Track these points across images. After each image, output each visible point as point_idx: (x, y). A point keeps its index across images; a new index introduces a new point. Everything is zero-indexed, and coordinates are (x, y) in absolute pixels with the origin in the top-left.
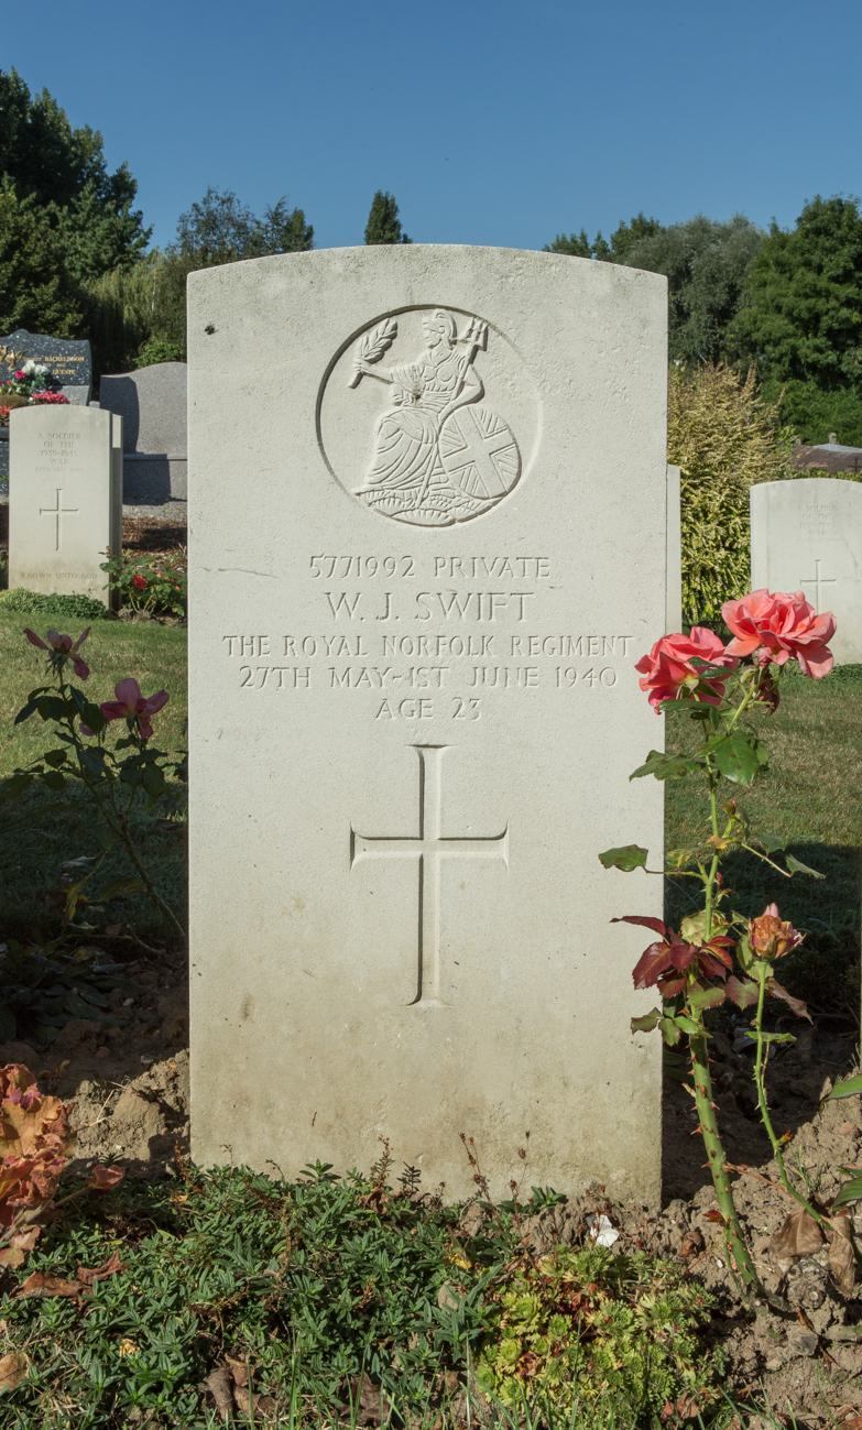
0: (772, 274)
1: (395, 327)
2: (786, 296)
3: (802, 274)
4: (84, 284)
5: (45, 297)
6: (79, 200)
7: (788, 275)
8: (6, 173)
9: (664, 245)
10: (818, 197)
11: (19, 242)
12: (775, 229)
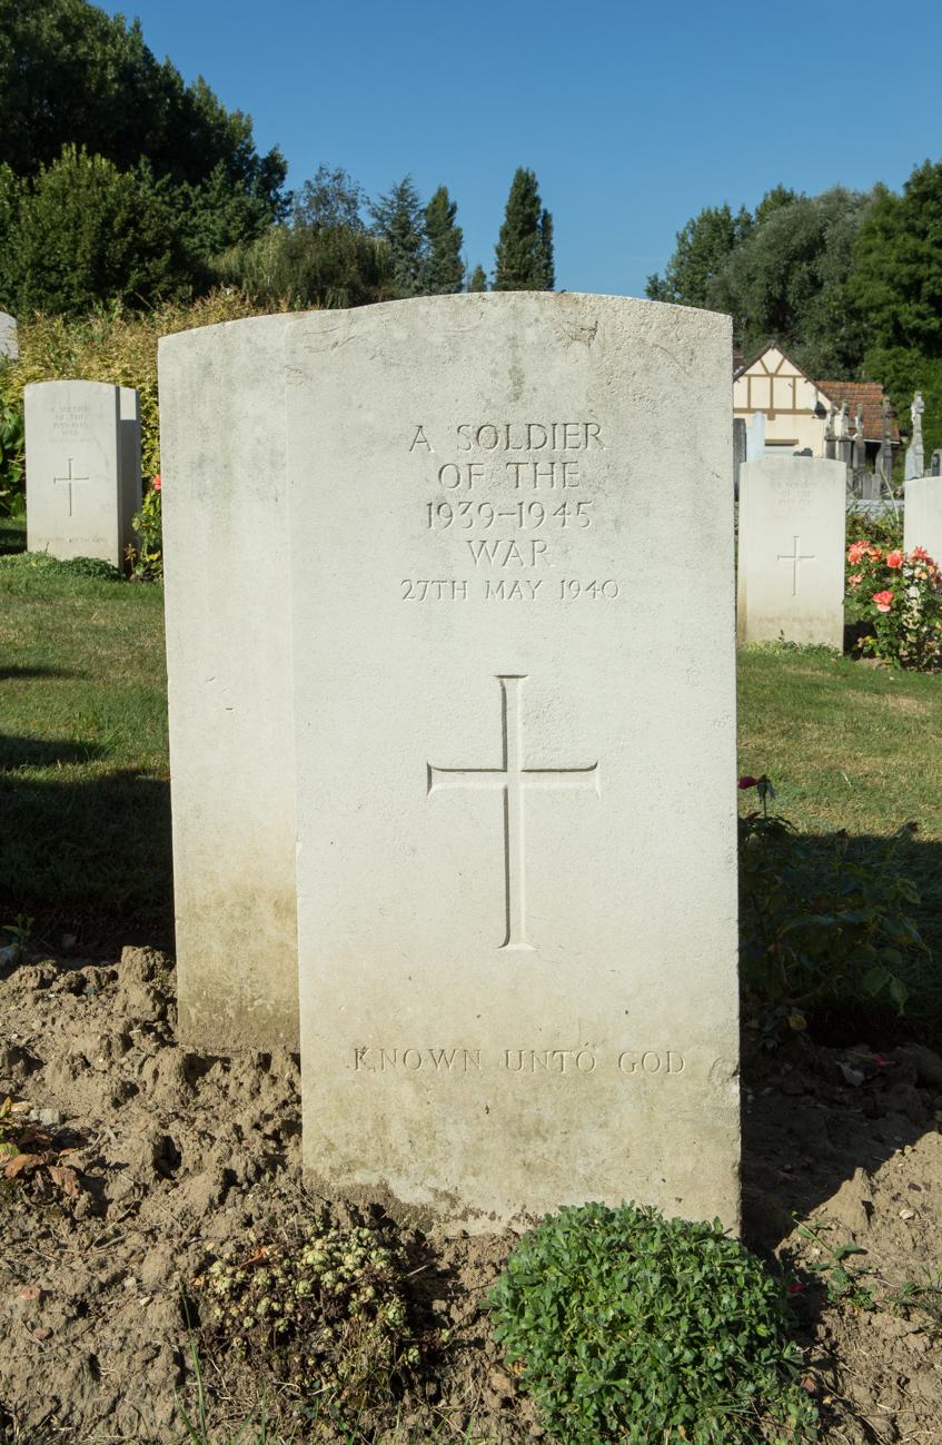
3: (904, 240)
5: (158, 270)
10: (928, 162)
11: (134, 218)
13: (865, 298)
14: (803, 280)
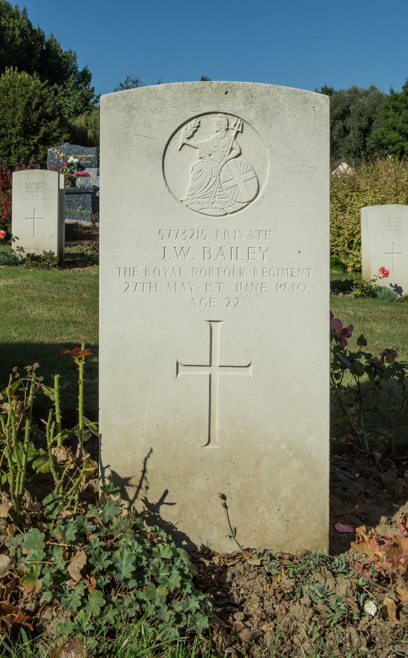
0: (391, 112)
1: (199, 122)
2: (398, 123)
4: (70, 121)
5: (53, 127)
6: (68, 82)
7: (399, 113)
8: (35, 71)
9: (337, 99)
12: (392, 91)
13: (386, 139)
14: (340, 129)
